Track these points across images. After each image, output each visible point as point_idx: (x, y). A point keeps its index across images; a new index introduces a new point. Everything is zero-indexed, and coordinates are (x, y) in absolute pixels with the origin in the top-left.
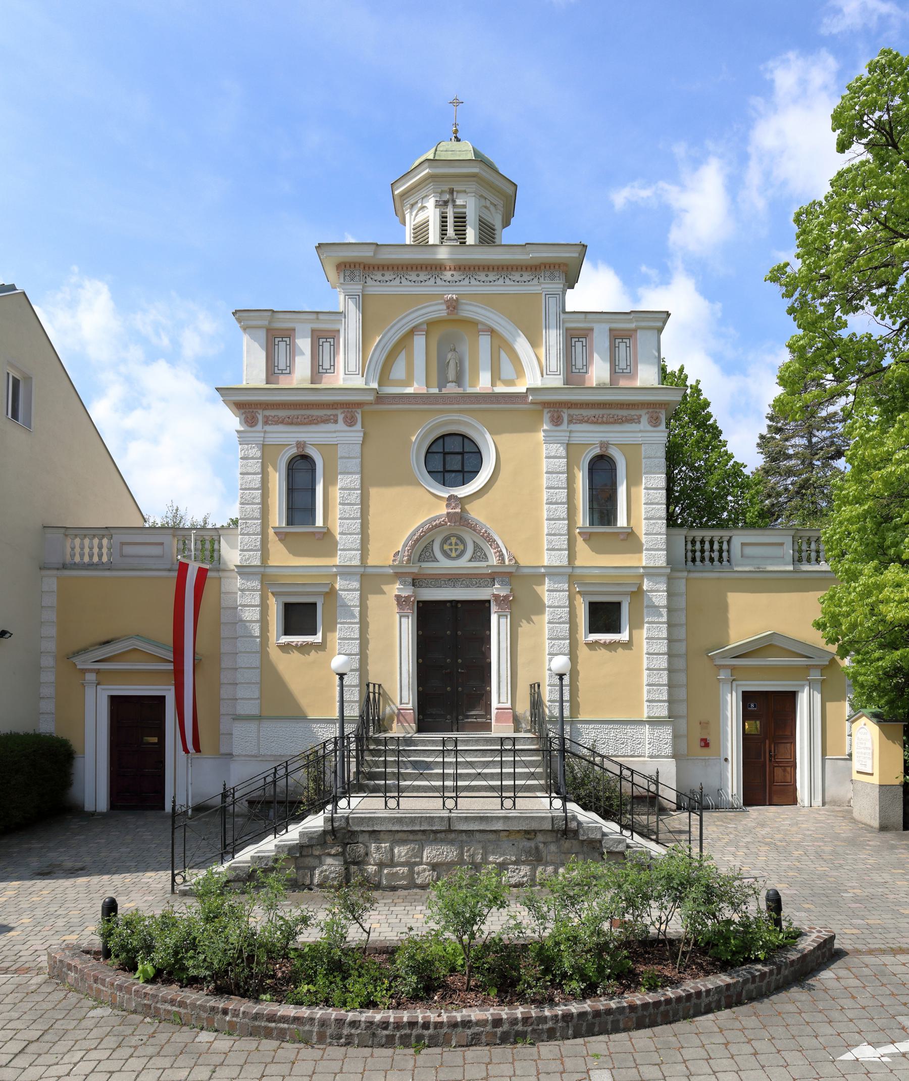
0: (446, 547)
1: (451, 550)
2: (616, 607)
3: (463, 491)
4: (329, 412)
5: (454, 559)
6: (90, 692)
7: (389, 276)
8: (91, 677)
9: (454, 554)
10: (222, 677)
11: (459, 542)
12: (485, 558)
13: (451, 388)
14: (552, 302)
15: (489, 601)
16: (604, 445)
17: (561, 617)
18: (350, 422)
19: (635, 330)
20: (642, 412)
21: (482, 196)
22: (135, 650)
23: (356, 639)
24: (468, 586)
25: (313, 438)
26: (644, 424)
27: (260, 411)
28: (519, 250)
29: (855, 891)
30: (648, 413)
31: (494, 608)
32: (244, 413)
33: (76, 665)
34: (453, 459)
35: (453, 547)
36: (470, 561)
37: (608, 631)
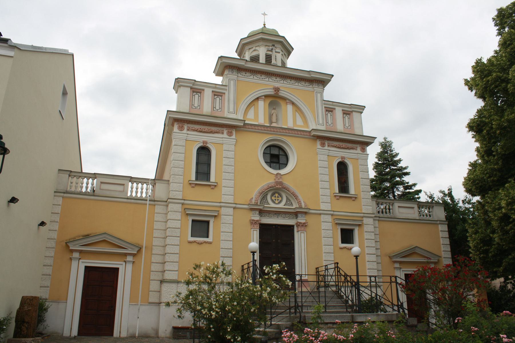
0: (273, 198)
2: (351, 231)
3: (283, 172)
4: (220, 129)
5: (277, 204)
6: (74, 264)
8: (76, 255)
9: (277, 202)
10: (152, 258)
13: (274, 125)
14: (319, 95)
15: (293, 226)
18: (230, 134)
19: (352, 112)
20: (358, 146)
21: (266, 46)
22: (104, 241)
23: (231, 241)
24: (284, 218)
25: (211, 140)
26: (225, 135)
27: (186, 124)
28: (307, 73)
33: (69, 247)
34: (276, 156)
35: (277, 198)
37: (350, 243)
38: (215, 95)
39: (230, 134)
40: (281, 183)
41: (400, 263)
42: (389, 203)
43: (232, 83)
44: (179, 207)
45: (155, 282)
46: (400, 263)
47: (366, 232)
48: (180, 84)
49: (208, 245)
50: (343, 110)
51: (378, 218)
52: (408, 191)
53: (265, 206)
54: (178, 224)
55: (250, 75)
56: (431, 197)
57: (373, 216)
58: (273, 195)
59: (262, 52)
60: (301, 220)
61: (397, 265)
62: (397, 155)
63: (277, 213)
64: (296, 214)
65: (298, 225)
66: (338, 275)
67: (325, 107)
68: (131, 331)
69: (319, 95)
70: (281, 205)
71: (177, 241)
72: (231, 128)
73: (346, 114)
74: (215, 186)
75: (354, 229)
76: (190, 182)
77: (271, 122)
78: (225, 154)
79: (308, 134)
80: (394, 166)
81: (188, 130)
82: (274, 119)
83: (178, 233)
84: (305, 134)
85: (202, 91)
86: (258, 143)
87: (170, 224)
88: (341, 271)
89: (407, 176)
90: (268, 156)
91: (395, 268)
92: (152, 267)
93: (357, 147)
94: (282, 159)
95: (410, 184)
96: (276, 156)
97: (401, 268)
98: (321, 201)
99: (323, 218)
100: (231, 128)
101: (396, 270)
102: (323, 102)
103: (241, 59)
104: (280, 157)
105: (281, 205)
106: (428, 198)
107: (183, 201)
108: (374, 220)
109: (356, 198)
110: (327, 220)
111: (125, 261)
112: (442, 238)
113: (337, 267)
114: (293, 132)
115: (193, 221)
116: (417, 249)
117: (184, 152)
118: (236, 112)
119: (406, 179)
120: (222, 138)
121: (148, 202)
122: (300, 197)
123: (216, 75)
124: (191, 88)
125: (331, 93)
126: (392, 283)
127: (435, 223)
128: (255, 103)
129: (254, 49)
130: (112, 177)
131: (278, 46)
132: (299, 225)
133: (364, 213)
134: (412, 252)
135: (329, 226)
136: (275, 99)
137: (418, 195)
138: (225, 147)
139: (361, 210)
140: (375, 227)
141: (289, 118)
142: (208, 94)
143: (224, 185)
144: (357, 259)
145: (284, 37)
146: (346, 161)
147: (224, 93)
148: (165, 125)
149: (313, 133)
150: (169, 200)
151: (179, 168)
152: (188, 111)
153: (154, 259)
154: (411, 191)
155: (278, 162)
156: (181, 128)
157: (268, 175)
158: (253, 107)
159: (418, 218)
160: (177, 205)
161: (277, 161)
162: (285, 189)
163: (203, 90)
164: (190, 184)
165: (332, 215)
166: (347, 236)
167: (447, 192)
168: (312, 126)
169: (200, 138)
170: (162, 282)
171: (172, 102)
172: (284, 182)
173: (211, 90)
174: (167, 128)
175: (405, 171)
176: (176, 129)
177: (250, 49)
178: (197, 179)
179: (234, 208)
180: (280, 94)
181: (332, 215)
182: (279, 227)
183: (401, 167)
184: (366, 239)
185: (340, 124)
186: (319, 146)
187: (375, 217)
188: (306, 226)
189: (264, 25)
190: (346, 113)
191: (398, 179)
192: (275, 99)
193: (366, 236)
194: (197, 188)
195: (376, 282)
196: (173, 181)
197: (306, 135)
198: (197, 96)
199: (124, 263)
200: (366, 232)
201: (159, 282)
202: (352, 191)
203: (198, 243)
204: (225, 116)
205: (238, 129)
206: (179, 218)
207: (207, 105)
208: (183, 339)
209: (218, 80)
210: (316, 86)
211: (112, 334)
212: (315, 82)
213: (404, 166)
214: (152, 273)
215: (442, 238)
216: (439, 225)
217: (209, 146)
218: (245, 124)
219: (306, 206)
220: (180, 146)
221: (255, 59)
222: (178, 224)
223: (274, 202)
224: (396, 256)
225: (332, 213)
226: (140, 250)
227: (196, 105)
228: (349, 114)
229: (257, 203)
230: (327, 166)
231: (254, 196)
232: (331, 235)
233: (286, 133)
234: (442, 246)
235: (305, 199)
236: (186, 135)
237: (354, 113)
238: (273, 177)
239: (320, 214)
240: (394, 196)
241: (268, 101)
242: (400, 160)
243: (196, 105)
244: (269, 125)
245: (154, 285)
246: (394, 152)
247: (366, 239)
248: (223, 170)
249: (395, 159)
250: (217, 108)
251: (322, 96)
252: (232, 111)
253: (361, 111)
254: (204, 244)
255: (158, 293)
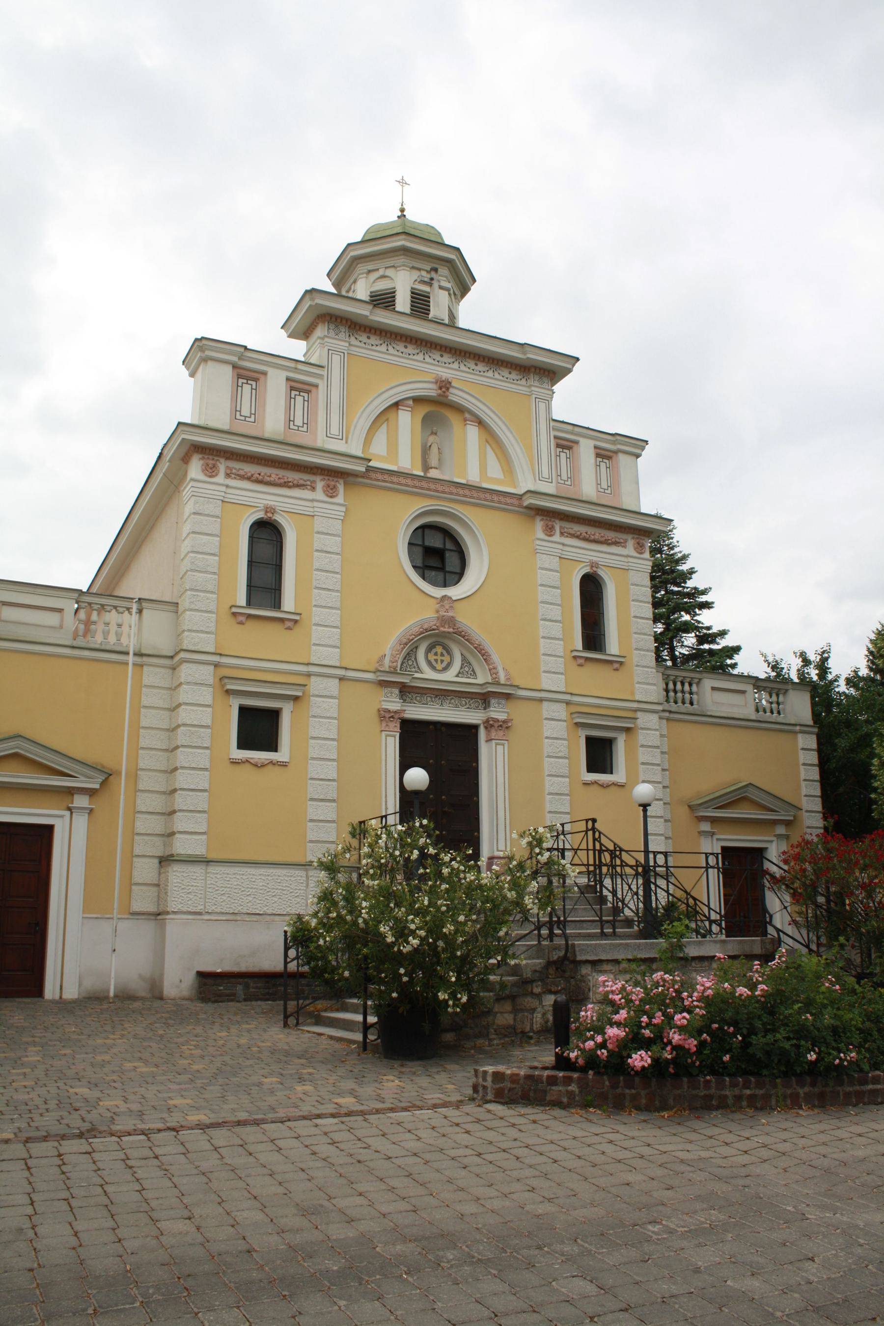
0: (431, 657)
1: (436, 660)
2: (274, 716)
3: (455, 592)
4: (306, 477)
7: (374, 340)
10: (138, 802)
11: (445, 652)
12: (474, 674)
13: (433, 473)
14: (542, 406)
15: (476, 727)
16: (268, 509)
17: (560, 751)
18: (331, 492)
19: (616, 452)
20: (629, 537)
21: (413, 268)
22: (16, 756)
23: (334, 760)
25: (288, 504)
26: (319, 494)
27: (222, 460)
29: (340, 1100)
30: (633, 538)
31: (482, 734)
32: (203, 458)
34: (438, 554)
35: (439, 658)
36: (457, 676)
38: (292, 389)
39: (331, 492)
40: (452, 621)
41: (713, 820)
42: (779, 689)
43: (336, 359)
44: (206, 673)
45: (147, 860)
46: (713, 820)
47: (642, 746)
48: (208, 353)
49: (277, 769)
50: (596, 447)
51: (667, 714)
52: (706, 646)
53: (417, 675)
54: (205, 716)
55: (451, 360)
56: (775, 667)
57: (660, 708)
58: (429, 649)
59: (403, 283)
60: (497, 712)
61: (706, 827)
62: (685, 557)
63: (442, 694)
64: (484, 699)
65: (489, 724)
66: (594, 850)
67: (556, 437)
68: (89, 984)
69: (542, 406)
70: (450, 675)
71: (202, 758)
72: (335, 476)
73: (603, 457)
74: (296, 621)
75: (615, 739)
76: (234, 610)
77: (426, 467)
78: (319, 541)
79: (515, 502)
80: (678, 585)
81: (228, 475)
82: (433, 461)
83: (204, 737)
84: (509, 501)
85: (262, 377)
86: (400, 517)
87: (185, 715)
88: (604, 840)
89: (705, 611)
90: (419, 551)
91: (701, 833)
92: (138, 824)
93: (626, 541)
94: (452, 561)
95: (714, 630)
96: (438, 554)
97: (713, 834)
98: (543, 669)
99: (548, 709)
100: (335, 476)
101: (702, 837)
102: (552, 424)
103: (339, 295)
104: (447, 554)
105: (450, 675)
106: (769, 670)
107: (216, 659)
108: (660, 718)
109: (621, 663)
110: (556, 715)
111: (69, 809)
112: (804, 764)
113: (593, 829)
114: (482, 496)
115: (243, 710)
116: (750, 789)
117: (218, 533)
118: (344, 436)
119: (705, 618)
120: (312, 501)
121: (131, 659)
122: (495, 657)
123: (290, 336)
124: (235, 367)
125: (568, 401)
126: (710, 870)
127: (790, 729)
128: (391, 415)
129: (381, 272)
130: (31, 590)
131: (444, 271)
132: (492, 726)
133: (639, 702)
134: (739, 797)
135: (559, 729)
136: (438, 409)
137: (731, 658)
138: (319, 524)
139: (633, 693)
140: (662, 736)
141: (470, 460)
142: (276, 383)
143: (315, 619)
144: (645, 811)
145: (458, 250)
146: (601, 573)
147: (316, 386)
148: (159, 457)
149: (528, 501)
150: (183, 655)
151: (206, 572)
152: (226, 427)
153: (145, 802)
154: (714, 647)
155: (442, 569)
156: (210, 471)
157: (420, 602)
158: (385, 425)
159: (753, 717)
160: (201, 667)
161: (439, 565)
162: (461, 635)
163: (265, 374)
164: (234, 614)
165: (568, 703)
166: (599, 754)
167: (813, 657)
168: (525, 483)
169: (256, 499)
170: (165, 860)
171: (180, 400)
172: (459, 619)
173: (284, 374)
174: (165, 466)
175: (703, 599)
176: (195, 469)
177: (369, 272)
178: (249, 603)
179: (342, 679)
180: (451, 398)
181: (217, 665)
182: (443, 729)
183: (695, 588)
184: (643, 764)
185: (589, 482)
186: (540, 534)
187: (663, 711)
188: (507, 728)
189: (402, 210)
190: (603, 455)
191: (686, 617)
192: (438, 409)
193: (643, 755)
194: (251, 625)
195: (667, 867)
196: (193, 606)
197: (512, 505)
198: (247, 388)
199: (68, 813)
200: (642, 746)
201: (156, 861)
202: (613, 645)
203: (602, 786)
204: (319, 444)
205: (350, 479)
206: (209, 701)
207: (273, 416)
208: (229, 1001)
209: (296, 349)
210: (537, 383)
211: (37, 989)
212: (535, 373)
213: (701, 588)
214: (136, 837)
215: (804, 764)
216: (800, 736)
217: (280, 519)
218: (370, 469)
219: (508, 679)
220: (208, 515)
221: (384, 300)
222: (205, 716)
223: (433, 668)
224: (705, 805)
225: (568, 697)
226: (108, 776)
227: (246, 411)
228: (609, 458)
229: (395, 669)
230: (558, 584)
231: (388, 652)
232: (564, 752)
233: (465, 496)
234: (803, 784)
235: (506, 665)
236: (223, 489)
237: (621, 456)
238: (433, 605)
239: (541, 700)
240: (673, 658)
241: (423, 410)
242: (692, 572)
243: (246, 411)
244: (422, 474)
245: (145, 870)
246: (676, 550)
247: (643, 764)
248: (314, 584)
249: (680, 568)
250: (299, 422)
251: (549, 409)
252: (336, 430)
253: (637, 451)
254: (270, 767)
255: (155, 889)
